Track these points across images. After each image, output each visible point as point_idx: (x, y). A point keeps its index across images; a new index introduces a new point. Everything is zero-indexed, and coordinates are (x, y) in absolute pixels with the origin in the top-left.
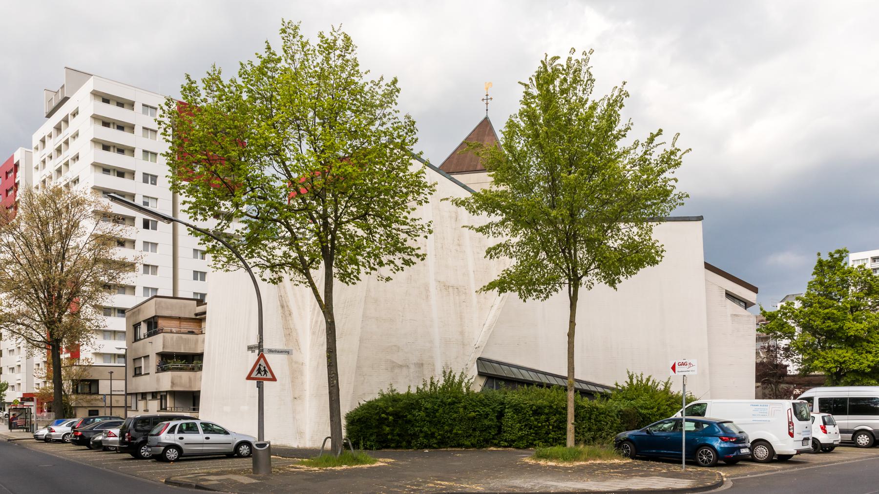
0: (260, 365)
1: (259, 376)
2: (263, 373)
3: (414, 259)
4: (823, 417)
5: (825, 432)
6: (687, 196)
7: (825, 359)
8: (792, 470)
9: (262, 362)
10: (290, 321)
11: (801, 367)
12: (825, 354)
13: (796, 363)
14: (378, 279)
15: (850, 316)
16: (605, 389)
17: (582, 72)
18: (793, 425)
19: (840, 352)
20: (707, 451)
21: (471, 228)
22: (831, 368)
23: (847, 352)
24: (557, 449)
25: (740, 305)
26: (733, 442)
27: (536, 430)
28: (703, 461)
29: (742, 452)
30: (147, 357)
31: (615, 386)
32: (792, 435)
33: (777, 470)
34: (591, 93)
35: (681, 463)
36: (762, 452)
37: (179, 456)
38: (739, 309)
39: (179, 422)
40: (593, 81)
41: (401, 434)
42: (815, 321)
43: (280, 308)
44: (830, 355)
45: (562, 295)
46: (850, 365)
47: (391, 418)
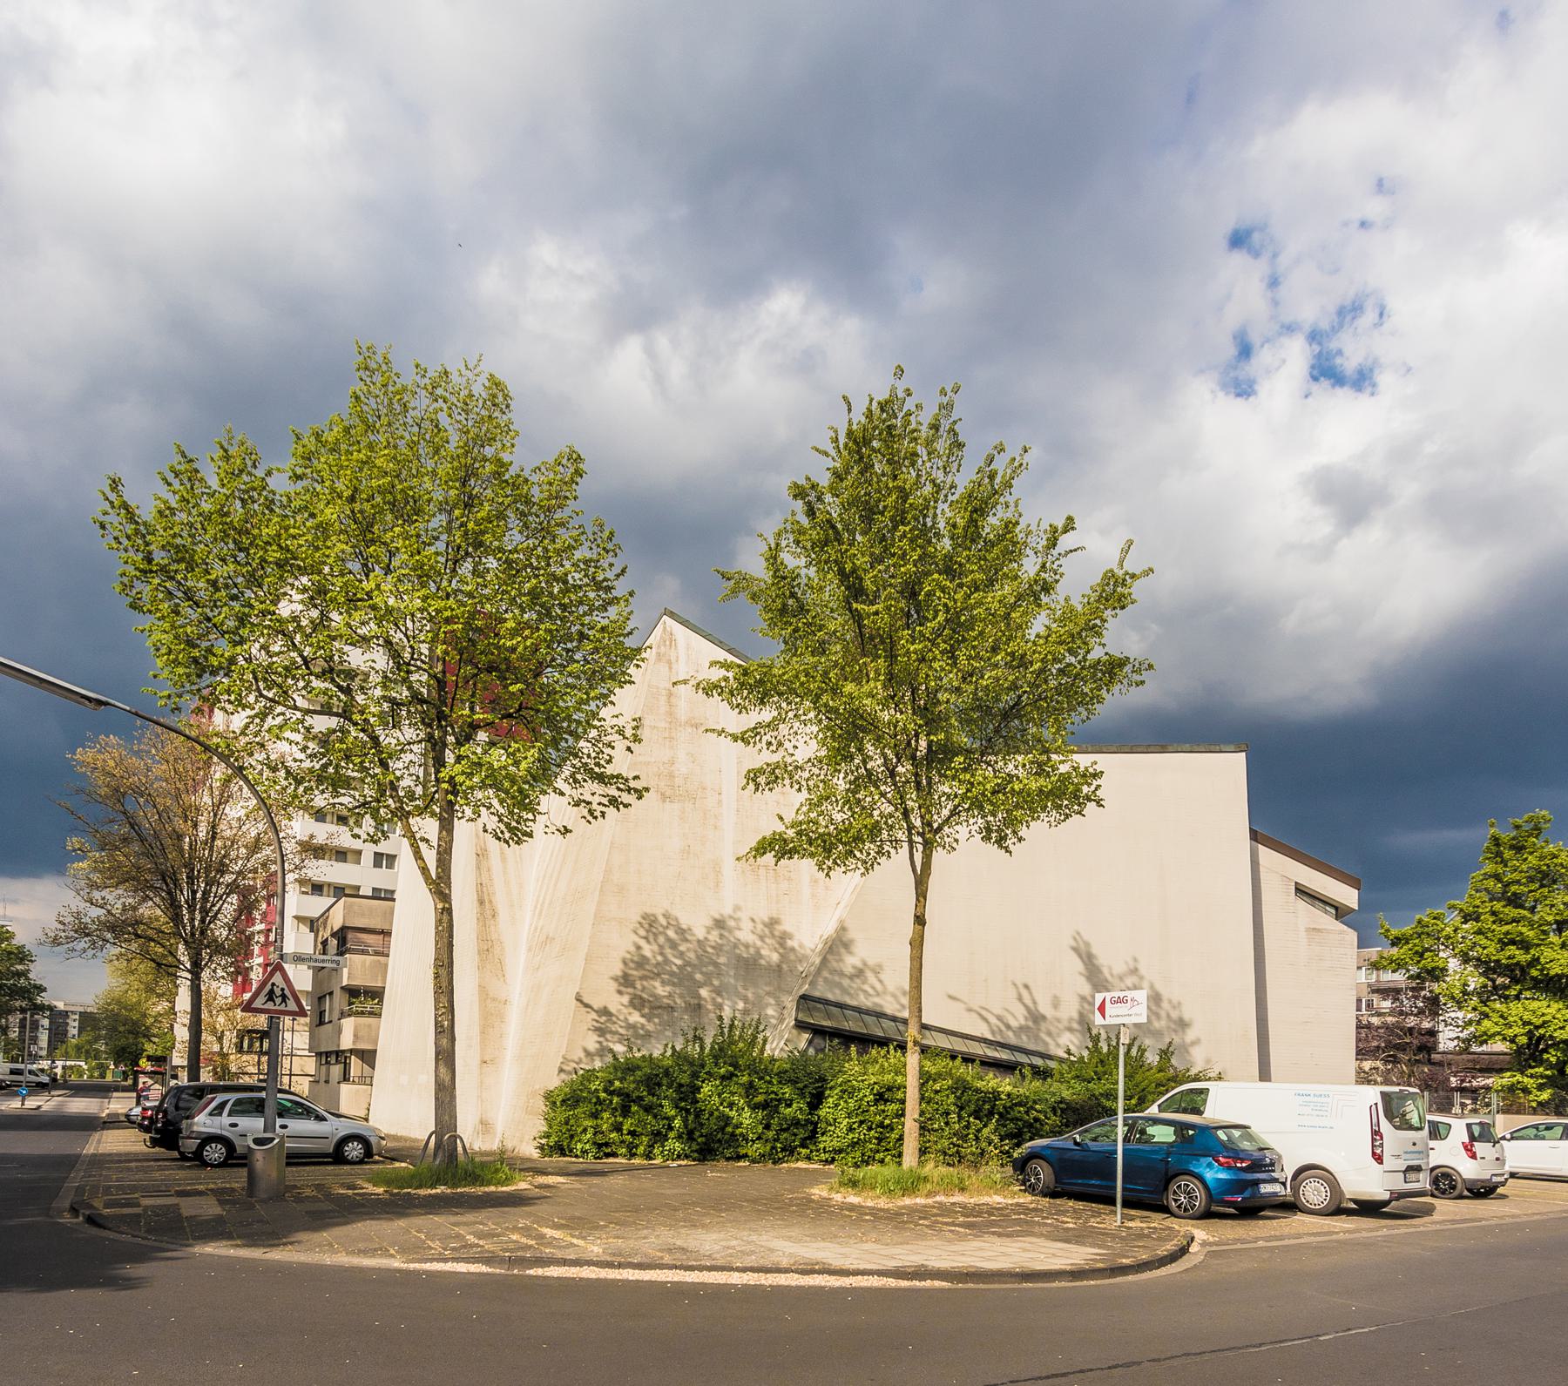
0: (273, 984)
1: (270, 1005)
2: (278, 1001)
3: (625, 798)
4: (1469, 1126)
5: (1474, 1156)
6: (1151, 667)
7: (1505, 1019)
8: (1375, 1234)
9: (277, 979)
10: (492, 928)
11: (1461, 1035)
12: (1505, 1010)
13: (1451, 1027)
14: (547, 830)
15: (1553, 938)
16: (1047, 1061)
17: (942, 429)
18: (1382, 1139)
19: (1534, 1005)
20: (1188, 1186)
21: (721, 732)
22: (1516, 1036)
23: (1549, 1006)
24: (888, 1171)
25: (1326, 912)
26: (1241, 1169)
27: (881, 1133)
28: (1179, 1207)
29: (1263, 1191)
30: (331, 994)
31: (1066, 1056)
32: (1379, 1159)
33: (1337, 1233)
34: (958, 471)
35: (1113, 1203)
36: (1314, 1194)
37: (226, 1159)
38: (1327, 921)
39: (233, 1097)
40: (960, 446)
41: (635, 1131)
42: (1484, 948)
43: (476, 903)
44: (1515, 1009)
45: (896, 867)
46: (1555, 1030)
47: (616, 1099)
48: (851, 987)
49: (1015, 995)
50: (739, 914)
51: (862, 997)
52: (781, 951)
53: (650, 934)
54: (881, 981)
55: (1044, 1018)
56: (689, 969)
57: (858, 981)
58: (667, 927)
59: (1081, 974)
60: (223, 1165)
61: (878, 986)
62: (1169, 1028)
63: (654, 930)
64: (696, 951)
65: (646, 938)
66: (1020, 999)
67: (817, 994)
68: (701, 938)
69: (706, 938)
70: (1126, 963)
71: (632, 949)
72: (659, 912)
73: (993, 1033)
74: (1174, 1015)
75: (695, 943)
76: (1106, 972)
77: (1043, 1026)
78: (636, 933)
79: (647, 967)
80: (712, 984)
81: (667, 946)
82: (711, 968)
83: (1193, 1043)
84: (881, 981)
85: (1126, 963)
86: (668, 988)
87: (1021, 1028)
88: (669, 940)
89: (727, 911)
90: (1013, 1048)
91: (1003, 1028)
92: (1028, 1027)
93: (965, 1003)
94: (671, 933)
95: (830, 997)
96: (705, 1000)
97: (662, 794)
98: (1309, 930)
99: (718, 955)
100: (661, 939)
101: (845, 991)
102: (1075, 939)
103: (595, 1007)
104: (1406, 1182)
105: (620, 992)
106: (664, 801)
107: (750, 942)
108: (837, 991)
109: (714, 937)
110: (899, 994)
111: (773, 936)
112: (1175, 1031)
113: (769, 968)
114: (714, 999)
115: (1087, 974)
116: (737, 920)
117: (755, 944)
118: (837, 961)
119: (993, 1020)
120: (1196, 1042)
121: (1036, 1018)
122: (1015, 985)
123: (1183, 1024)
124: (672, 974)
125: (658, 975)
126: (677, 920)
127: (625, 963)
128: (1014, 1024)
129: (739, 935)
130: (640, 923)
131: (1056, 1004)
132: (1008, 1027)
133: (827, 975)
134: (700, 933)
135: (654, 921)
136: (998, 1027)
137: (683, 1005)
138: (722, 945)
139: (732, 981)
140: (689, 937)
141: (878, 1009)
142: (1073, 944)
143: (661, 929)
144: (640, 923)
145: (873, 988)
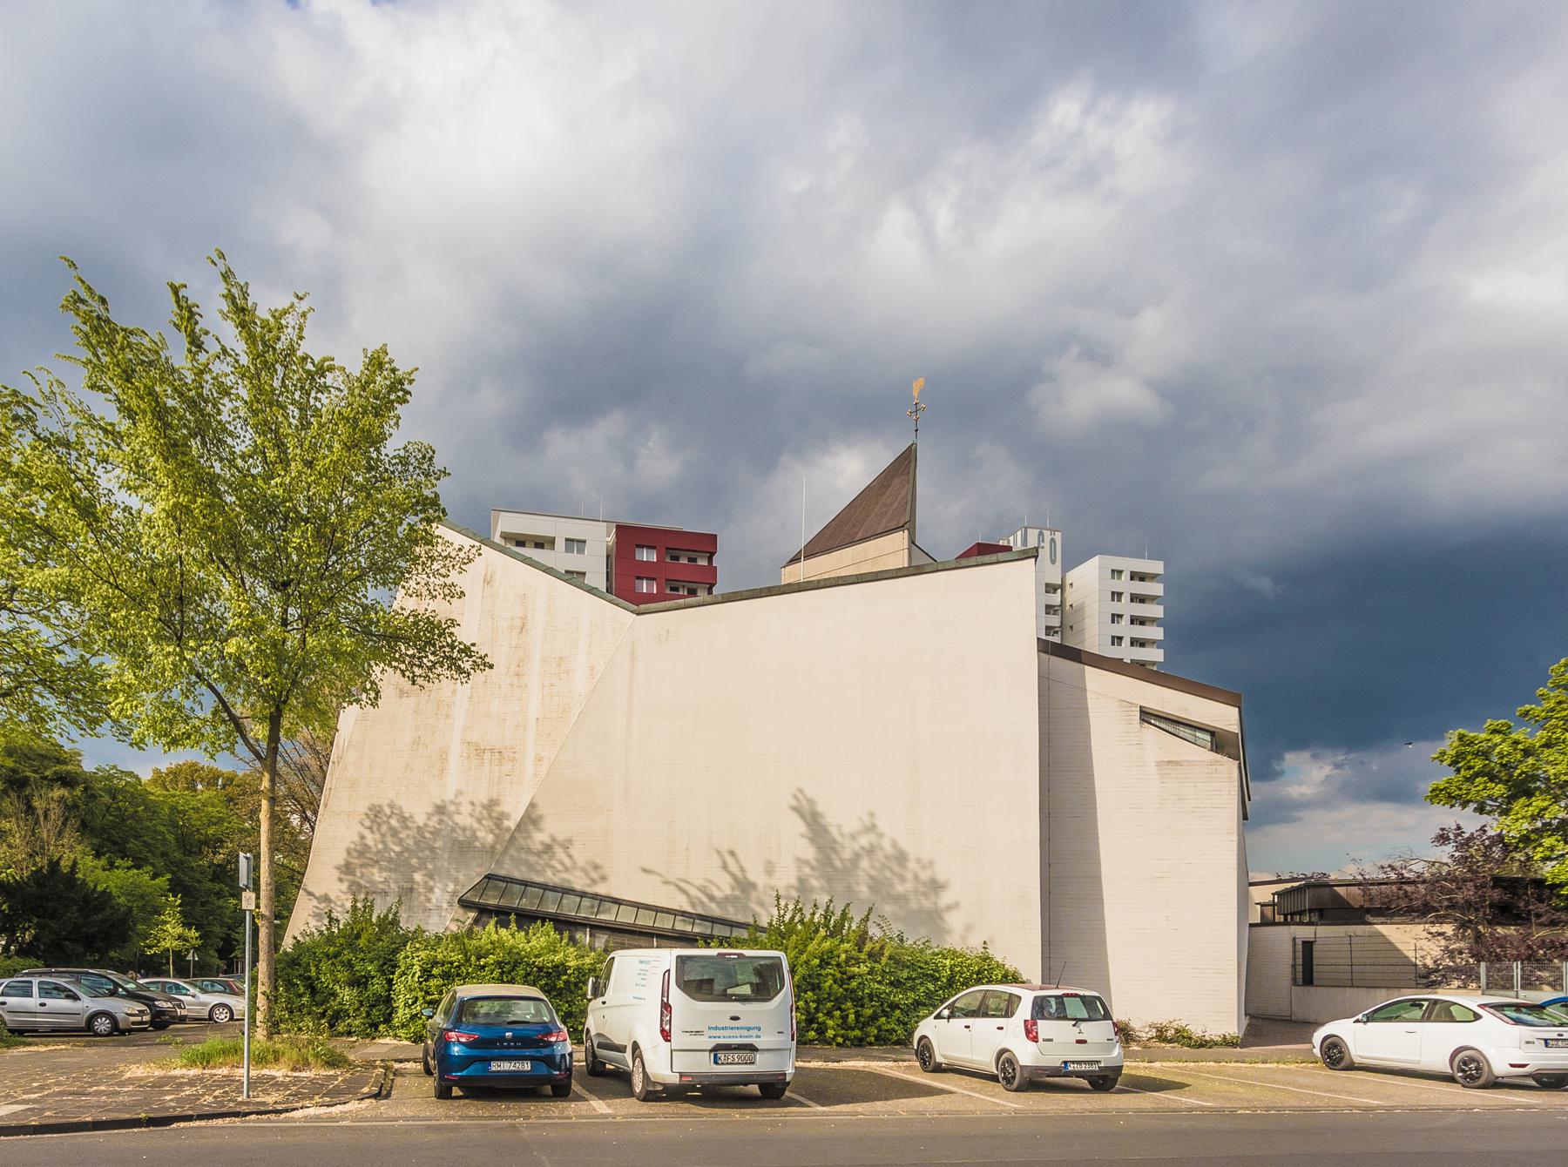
32: (666, 1035)
38: (1198, 754)
48: (537, 863)
49: (718, 863)
50: (460, 799)
51: (549, 873)
52: (497, 832)
53: (375, 824)
54: (570, 856)
55: (753, 886)
56: (406, 855)
57: (546, 857)
58: (390, 816)
59: (802, 836)
60: (110, 1034)
61: (568, 862)
62: (916, 891)
63: (378, 820)
64: (414, 838)
65: (370, 828)
66: (725, 867)
67: (503, 873)
68: (421, 824)
69: (426, 825)
70: (860, 819)
71: (357, 839)
72: (384, 802)
73: (693, 905)
74: (925, 876)
75: (415, 830)
76: (834, 832)
77: (754, 894)
78: (362, 825)
79: (369, 855)
80: (426, 868)
81: (388, 835)
82: (427, 853)
83: (949, 908)
84: (570, 856)
85: (860, 819)
86: (384, 874)
87: (727, 898)
88: (391, 828)
89: (449, 796)
90: (713, 920)
91: (705, 900)
92: (736, 898)
93: (661, 875)
94: (394, 822)
95: (517, 875)
96: (418, 884)
97: (401, 690)
98: (1159, 764)
99: (435, 840)
100: (384, 828)
101: (531, 867)
102: (796, 797)
103: (317, 895)
104: (716, 1063)
105: (341, 880)
106: (401, 697)
107: (468, 825)
108: (524, 869)
109: (434, 822)
110: (589, 868)
111: (491, 818)
112: (925, 895)
113: (483, 850)
114: (426, 882)
115: (810, 836)
116: (458, 805)
117: (471, 826)
118: (525, 838)
119: (694, 892)
120: (955, 906)
121: (745, 886)
122: (718, 852)
123: (936, 886)
124: (390, 860)
125: (377, 862)
126: (400, 808)
127: (349, 852)
128: (717, 894)
129: (457, 818)
130: (367, 814)
131: (770, 869)
132: (712, 898)
133: (515, 854)
134: (420, 820)
135: (379, 812)
136: (699, 899)
137: (397, 890)
138: (441, 830)
139: (446, 864)
140: (410, 825)
141: (566, 885)
142: (794, 803)
143: (385, 819)
144: (367, 814)
145: (562, 863)
